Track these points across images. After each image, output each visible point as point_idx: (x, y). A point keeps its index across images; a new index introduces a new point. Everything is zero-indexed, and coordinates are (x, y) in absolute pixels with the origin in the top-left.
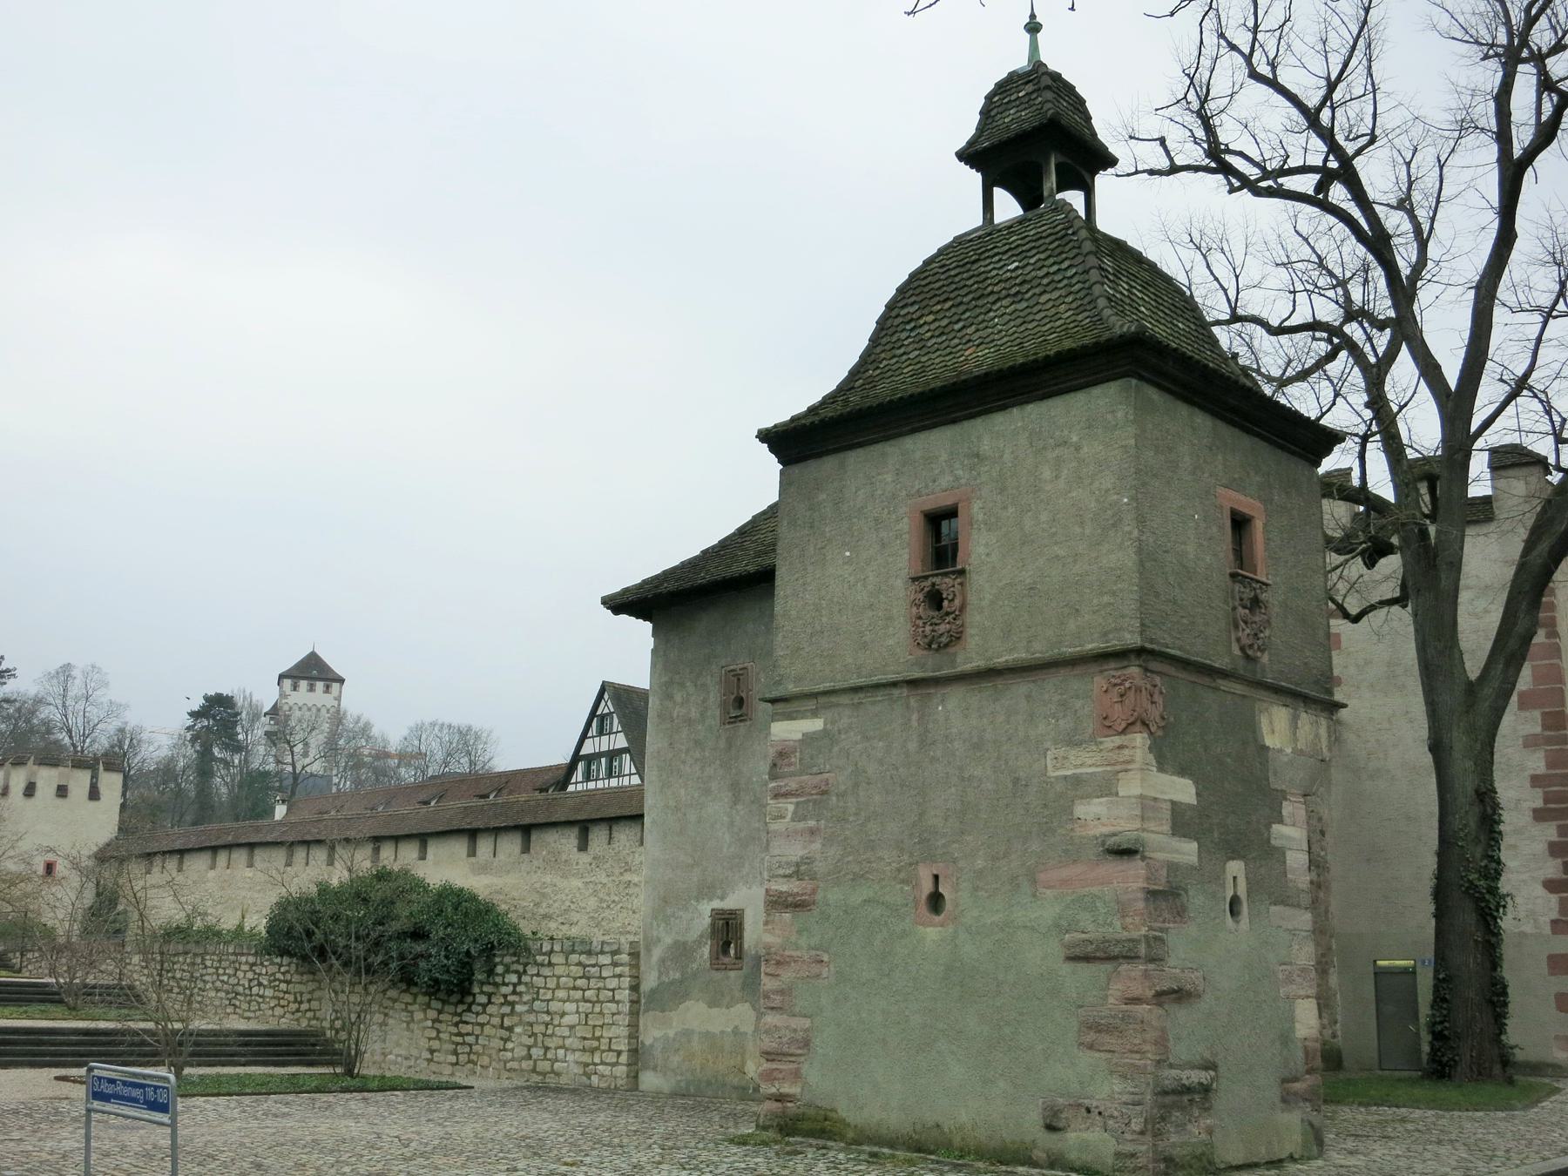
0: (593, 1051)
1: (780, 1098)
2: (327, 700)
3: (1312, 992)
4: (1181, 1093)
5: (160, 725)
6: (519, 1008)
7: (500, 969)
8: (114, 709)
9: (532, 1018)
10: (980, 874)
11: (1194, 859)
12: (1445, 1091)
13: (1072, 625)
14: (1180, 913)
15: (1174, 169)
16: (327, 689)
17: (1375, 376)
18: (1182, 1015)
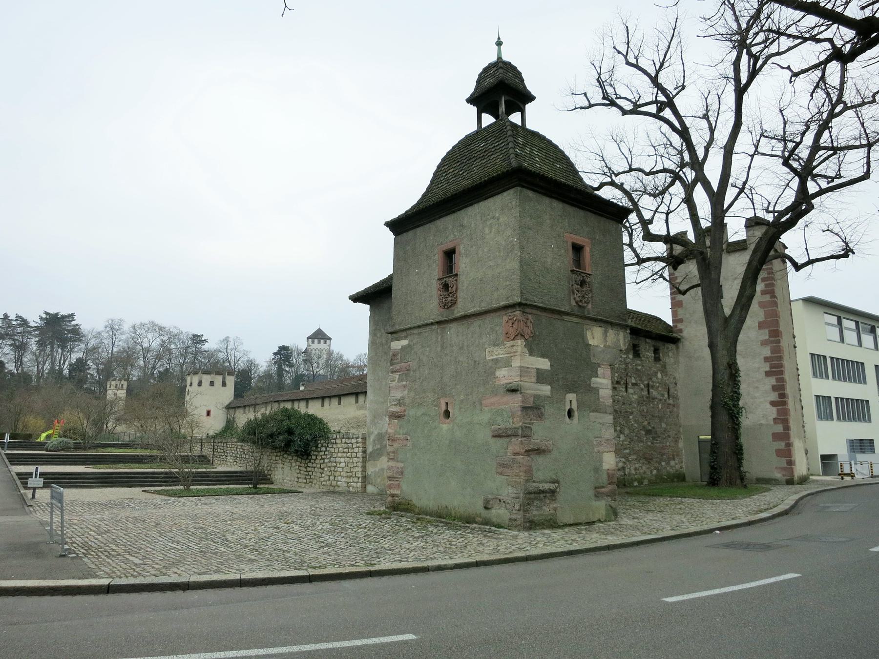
0: (350, 477)
1: (393, 496)
2: (326, 347)
3: (613, 449)
4: (539, 493)
5: (262, 358)
6: (326, 461)
7: (320, 445)
8: (245, 353)
9: (330, 464)
10: (462, 401)
11: (549, 393)
12: (714, 491)
13: (496, 295)
14: (541, 416)
15: (591, 106)
16: (325, 343)
17: (689, 189)
18: (540, 459)
